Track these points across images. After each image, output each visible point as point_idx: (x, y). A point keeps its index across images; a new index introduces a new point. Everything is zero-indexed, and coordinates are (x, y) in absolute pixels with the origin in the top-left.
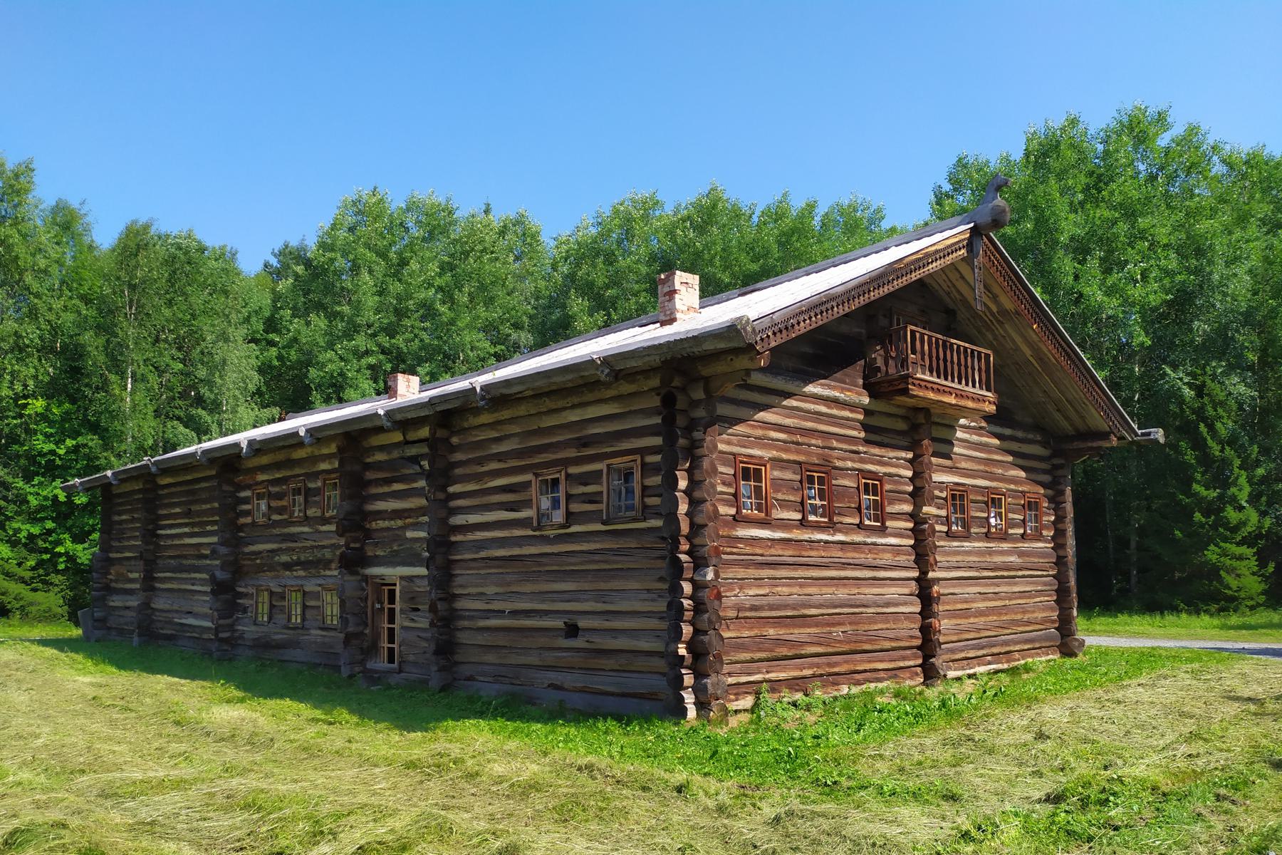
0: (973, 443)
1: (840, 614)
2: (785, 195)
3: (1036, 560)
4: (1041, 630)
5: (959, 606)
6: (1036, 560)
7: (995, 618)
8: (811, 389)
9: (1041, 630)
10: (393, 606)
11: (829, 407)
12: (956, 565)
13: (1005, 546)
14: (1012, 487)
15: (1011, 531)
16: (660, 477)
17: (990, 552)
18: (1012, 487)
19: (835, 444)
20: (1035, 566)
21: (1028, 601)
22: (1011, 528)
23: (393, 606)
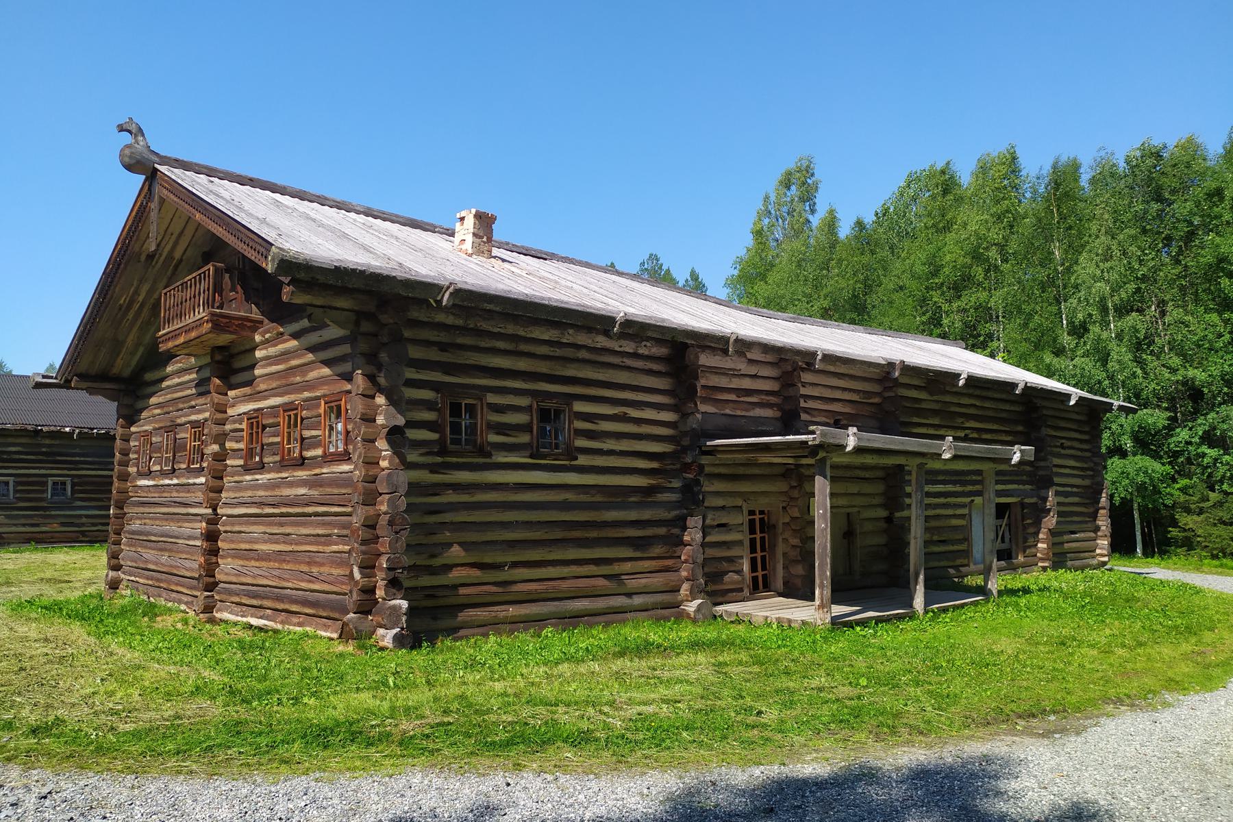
0: (276, 356)
1: (164, 542)
2: (948, 163)
3: (336, 491)
4: (328, 593)
5: (244, 546)
6: (336, 491)
7: (277, 565)
8: (169, 369)
9: (328, 593)
10: (751, 517)
11: (179, 377)
12: (249, 500)
13: (302, 474)
14: (306, 394)
15: (308, 454)
16: (688, 439)
17: (284, 483)
18: (306, 394)
19: (181, 406)
20: (327, 499)
21: (321, 548)
22: (308, 449)
23: (751, 517)
